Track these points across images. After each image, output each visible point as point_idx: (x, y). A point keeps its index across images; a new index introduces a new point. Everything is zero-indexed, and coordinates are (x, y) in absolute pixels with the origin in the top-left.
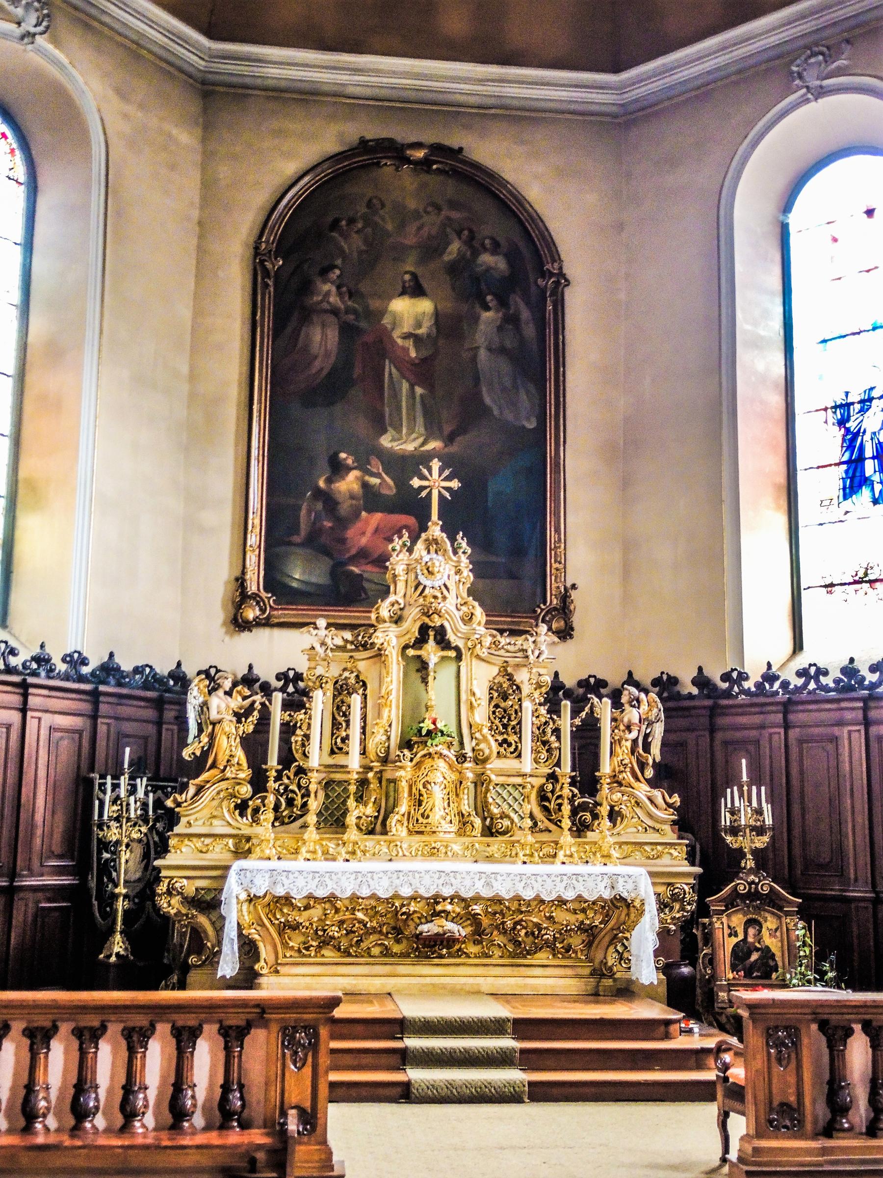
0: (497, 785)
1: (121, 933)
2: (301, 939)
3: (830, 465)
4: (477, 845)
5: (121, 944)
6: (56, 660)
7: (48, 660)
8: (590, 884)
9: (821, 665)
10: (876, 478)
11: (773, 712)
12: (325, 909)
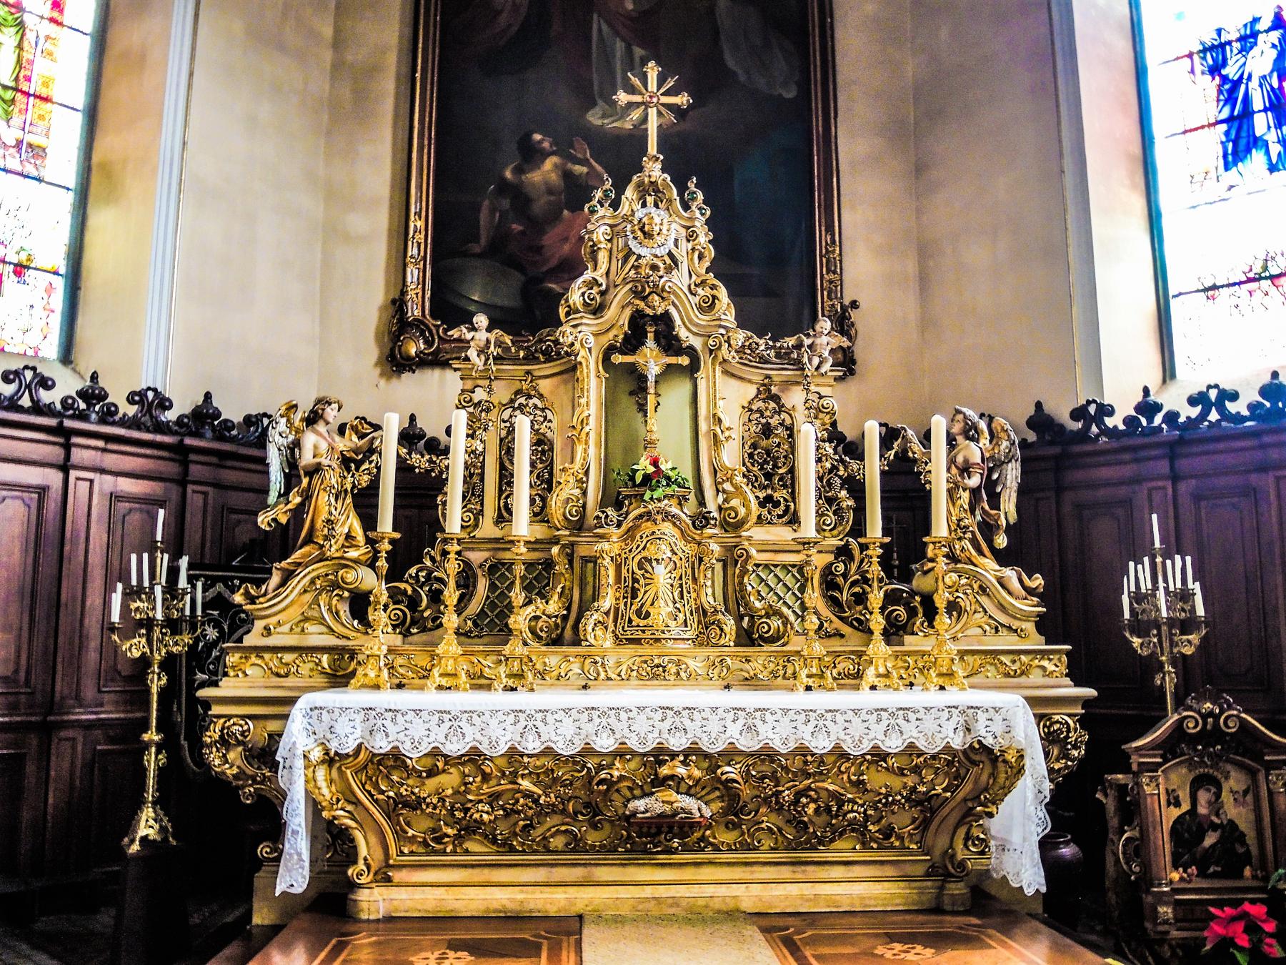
0: (758, 566)
1: (154, 803)
2: (427, 824)
3: (1203, 127)
4: (729, 661)
5: (151, 822)
6: (117, 397)
7: (103, 396)
8: (929, 725)
9: (1227, 385)
10: (1272, 137)
11: (1156, 458)
12: (465, 775)
